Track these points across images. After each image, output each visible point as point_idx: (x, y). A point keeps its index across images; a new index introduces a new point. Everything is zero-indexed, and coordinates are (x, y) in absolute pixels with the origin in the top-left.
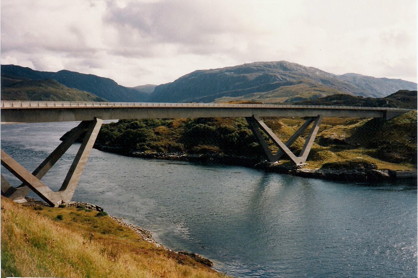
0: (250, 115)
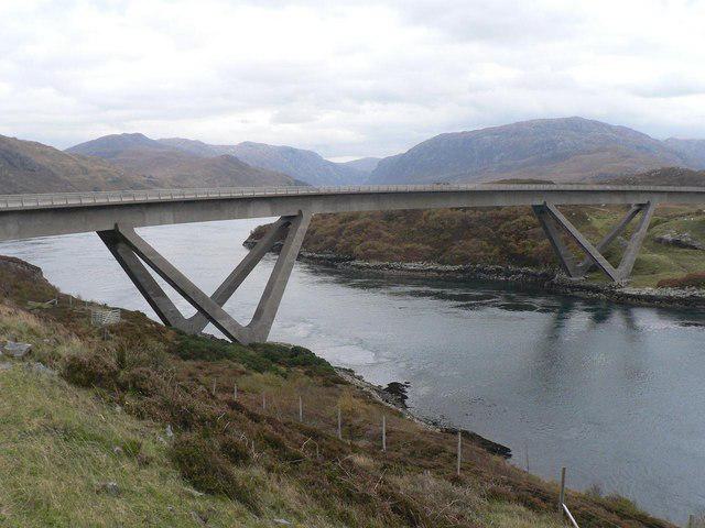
0: (538, 202)
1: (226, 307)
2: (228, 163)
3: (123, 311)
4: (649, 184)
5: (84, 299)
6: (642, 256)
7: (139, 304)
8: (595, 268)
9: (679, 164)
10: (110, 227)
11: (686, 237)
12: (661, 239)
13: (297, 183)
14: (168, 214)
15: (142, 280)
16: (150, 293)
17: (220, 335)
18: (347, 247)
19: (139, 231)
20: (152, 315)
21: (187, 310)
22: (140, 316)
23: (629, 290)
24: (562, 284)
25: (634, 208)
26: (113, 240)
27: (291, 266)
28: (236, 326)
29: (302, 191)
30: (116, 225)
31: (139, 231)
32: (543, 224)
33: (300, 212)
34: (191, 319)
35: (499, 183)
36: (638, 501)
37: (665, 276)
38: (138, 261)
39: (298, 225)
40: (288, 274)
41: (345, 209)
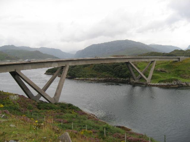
0: (127, 61)
1: (47, 92)
2: (36, 53)
3: (19, 95)
4: (148, 56)
5: (13, 93)
6: (154, 75)
7: (22, 93)
8: (141, 78)
9: (153, 51)
10: (13, 70)
11: (163, 69)
12: (157, 70)
13: (56, 58)
14: (30, 66)
15: (22, 86)
16: (25, 89)
17: (44, 100)
18: (176, 73)
19: (22, 71)
20: (26, 96)
21: (35, 93)
22: (22, 96)
23: (151, 84)
24: (133, 82)
25: (150, 62)
26: (15, 75)
27: (64, 80)
28: (50, 98)
29: (58, 60)
30: (15, 70)
31: (22, 71)
32: (128, 67)
33: (66, 65)
34: (36, 96)
35: (112, 56)
36: (8, 92)
37: (159, 79)
38: (21, 79)
39: (154, 63)
40: (63, 82)
41: (102, 62)
